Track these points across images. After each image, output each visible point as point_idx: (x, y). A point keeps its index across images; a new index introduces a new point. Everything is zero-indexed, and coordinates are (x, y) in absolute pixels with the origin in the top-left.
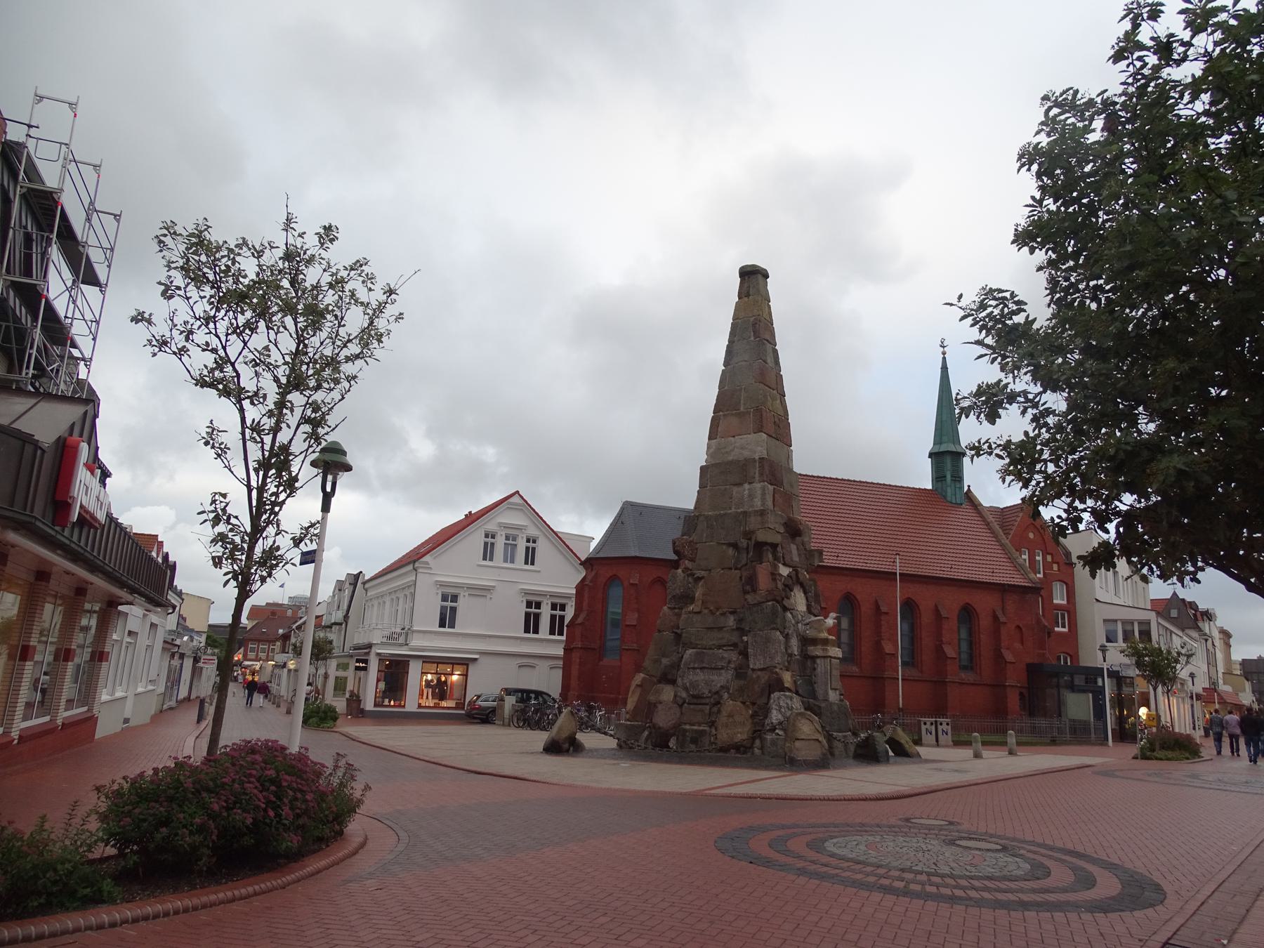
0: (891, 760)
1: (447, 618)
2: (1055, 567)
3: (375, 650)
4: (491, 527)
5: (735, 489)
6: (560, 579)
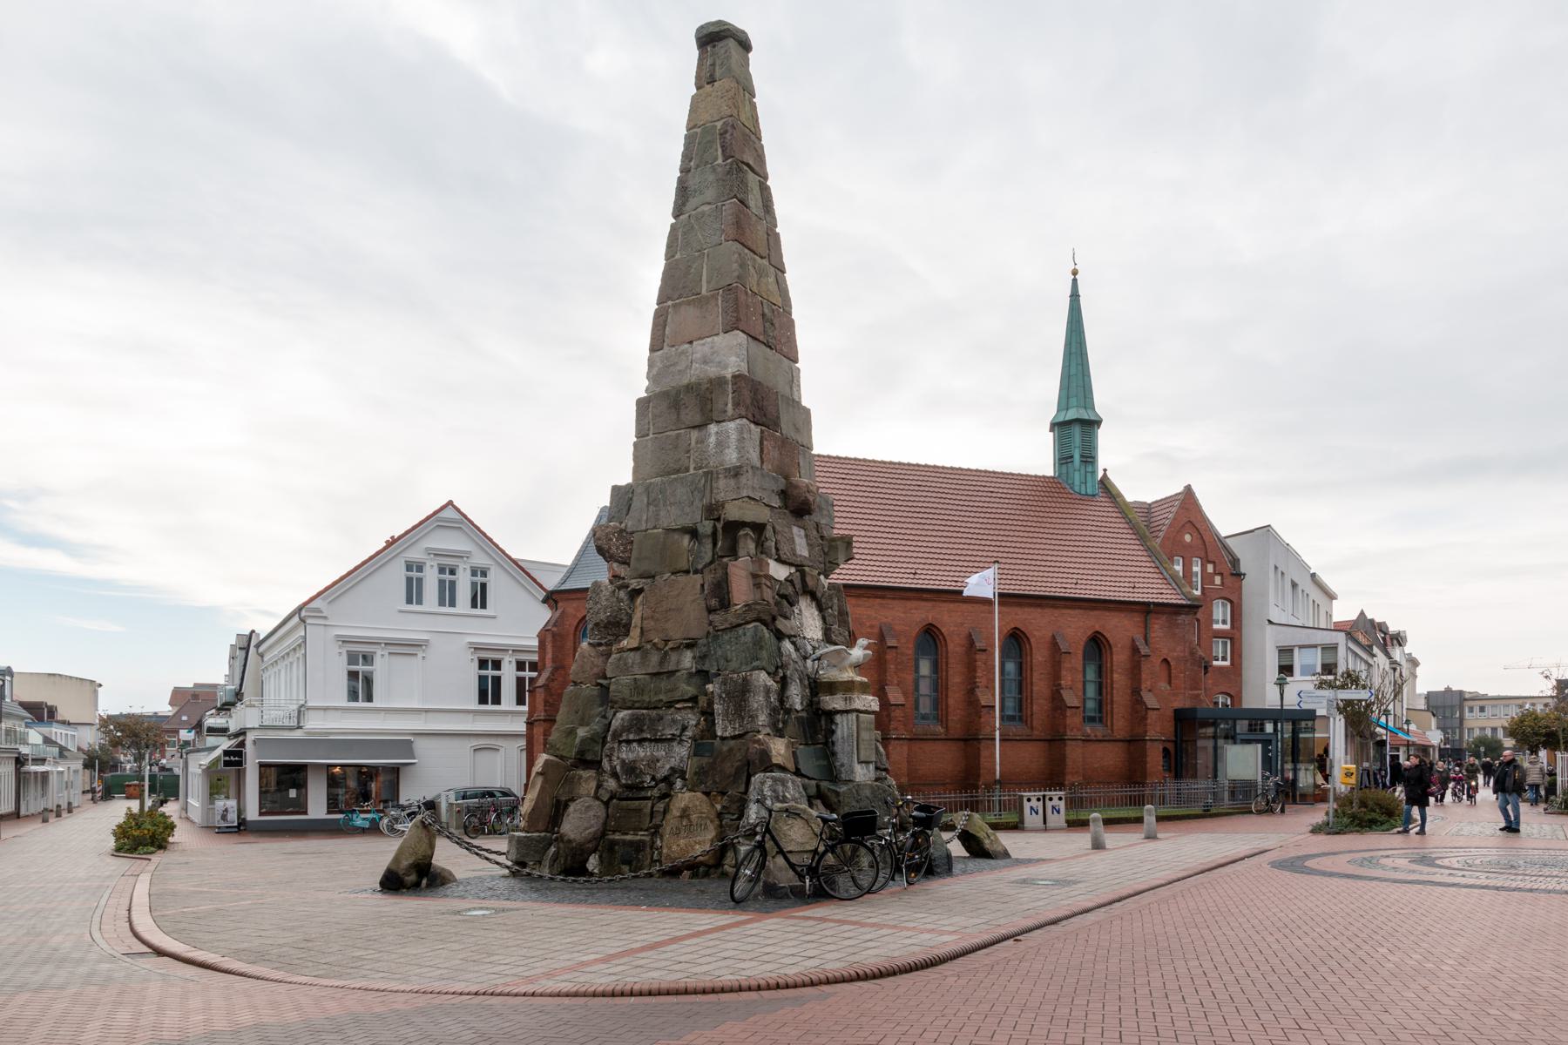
0: (957, 867)
1: (361, 686)
2: (1218, 580)
3: (250, 737)
4: (415, 554)
5: (694, 434)
6: (519, 624)
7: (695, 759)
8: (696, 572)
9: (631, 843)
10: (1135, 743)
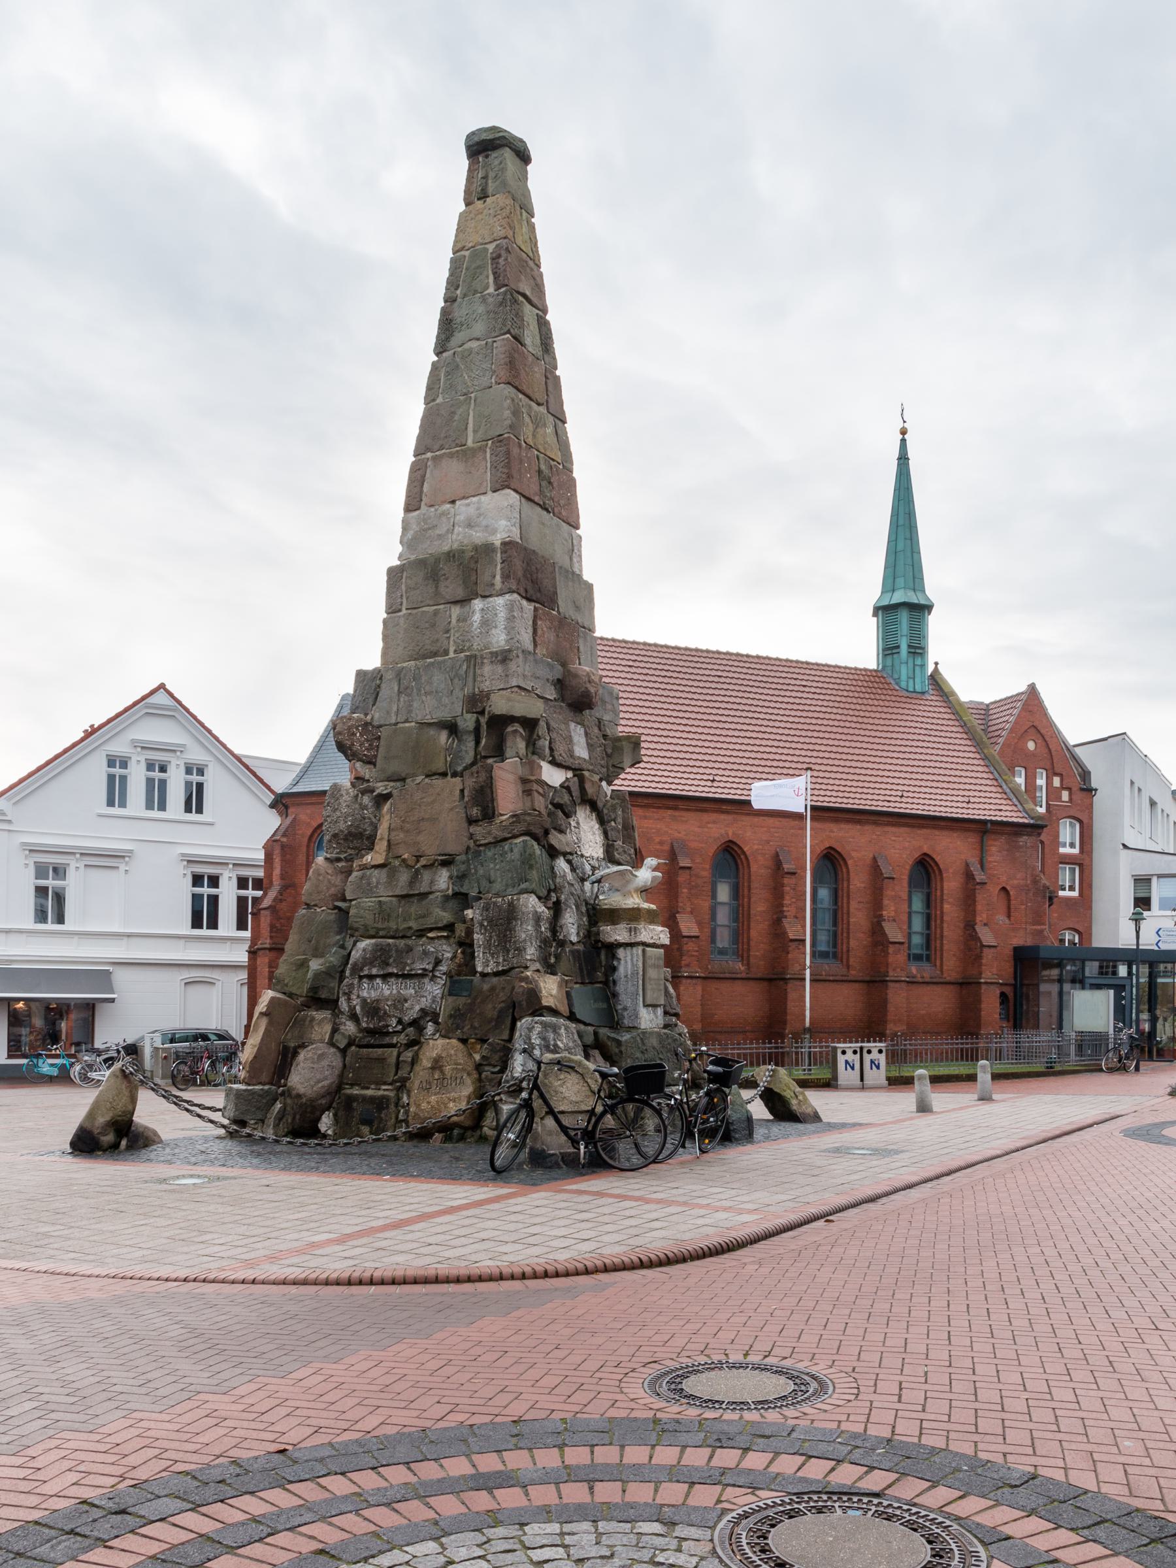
2: (1065, 795)
4: (119, 747)
5: (456, 611)
6: (241, 832)
7: (450, 999)
8: (455, 775)
9: (372, 1099)
10: (968, 986)
